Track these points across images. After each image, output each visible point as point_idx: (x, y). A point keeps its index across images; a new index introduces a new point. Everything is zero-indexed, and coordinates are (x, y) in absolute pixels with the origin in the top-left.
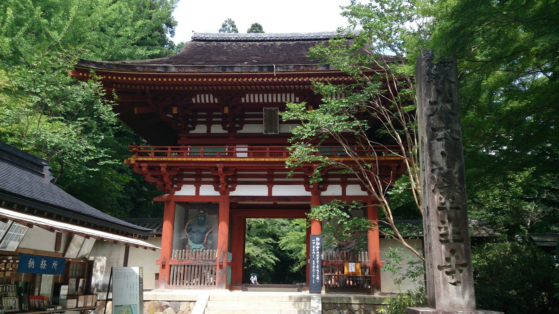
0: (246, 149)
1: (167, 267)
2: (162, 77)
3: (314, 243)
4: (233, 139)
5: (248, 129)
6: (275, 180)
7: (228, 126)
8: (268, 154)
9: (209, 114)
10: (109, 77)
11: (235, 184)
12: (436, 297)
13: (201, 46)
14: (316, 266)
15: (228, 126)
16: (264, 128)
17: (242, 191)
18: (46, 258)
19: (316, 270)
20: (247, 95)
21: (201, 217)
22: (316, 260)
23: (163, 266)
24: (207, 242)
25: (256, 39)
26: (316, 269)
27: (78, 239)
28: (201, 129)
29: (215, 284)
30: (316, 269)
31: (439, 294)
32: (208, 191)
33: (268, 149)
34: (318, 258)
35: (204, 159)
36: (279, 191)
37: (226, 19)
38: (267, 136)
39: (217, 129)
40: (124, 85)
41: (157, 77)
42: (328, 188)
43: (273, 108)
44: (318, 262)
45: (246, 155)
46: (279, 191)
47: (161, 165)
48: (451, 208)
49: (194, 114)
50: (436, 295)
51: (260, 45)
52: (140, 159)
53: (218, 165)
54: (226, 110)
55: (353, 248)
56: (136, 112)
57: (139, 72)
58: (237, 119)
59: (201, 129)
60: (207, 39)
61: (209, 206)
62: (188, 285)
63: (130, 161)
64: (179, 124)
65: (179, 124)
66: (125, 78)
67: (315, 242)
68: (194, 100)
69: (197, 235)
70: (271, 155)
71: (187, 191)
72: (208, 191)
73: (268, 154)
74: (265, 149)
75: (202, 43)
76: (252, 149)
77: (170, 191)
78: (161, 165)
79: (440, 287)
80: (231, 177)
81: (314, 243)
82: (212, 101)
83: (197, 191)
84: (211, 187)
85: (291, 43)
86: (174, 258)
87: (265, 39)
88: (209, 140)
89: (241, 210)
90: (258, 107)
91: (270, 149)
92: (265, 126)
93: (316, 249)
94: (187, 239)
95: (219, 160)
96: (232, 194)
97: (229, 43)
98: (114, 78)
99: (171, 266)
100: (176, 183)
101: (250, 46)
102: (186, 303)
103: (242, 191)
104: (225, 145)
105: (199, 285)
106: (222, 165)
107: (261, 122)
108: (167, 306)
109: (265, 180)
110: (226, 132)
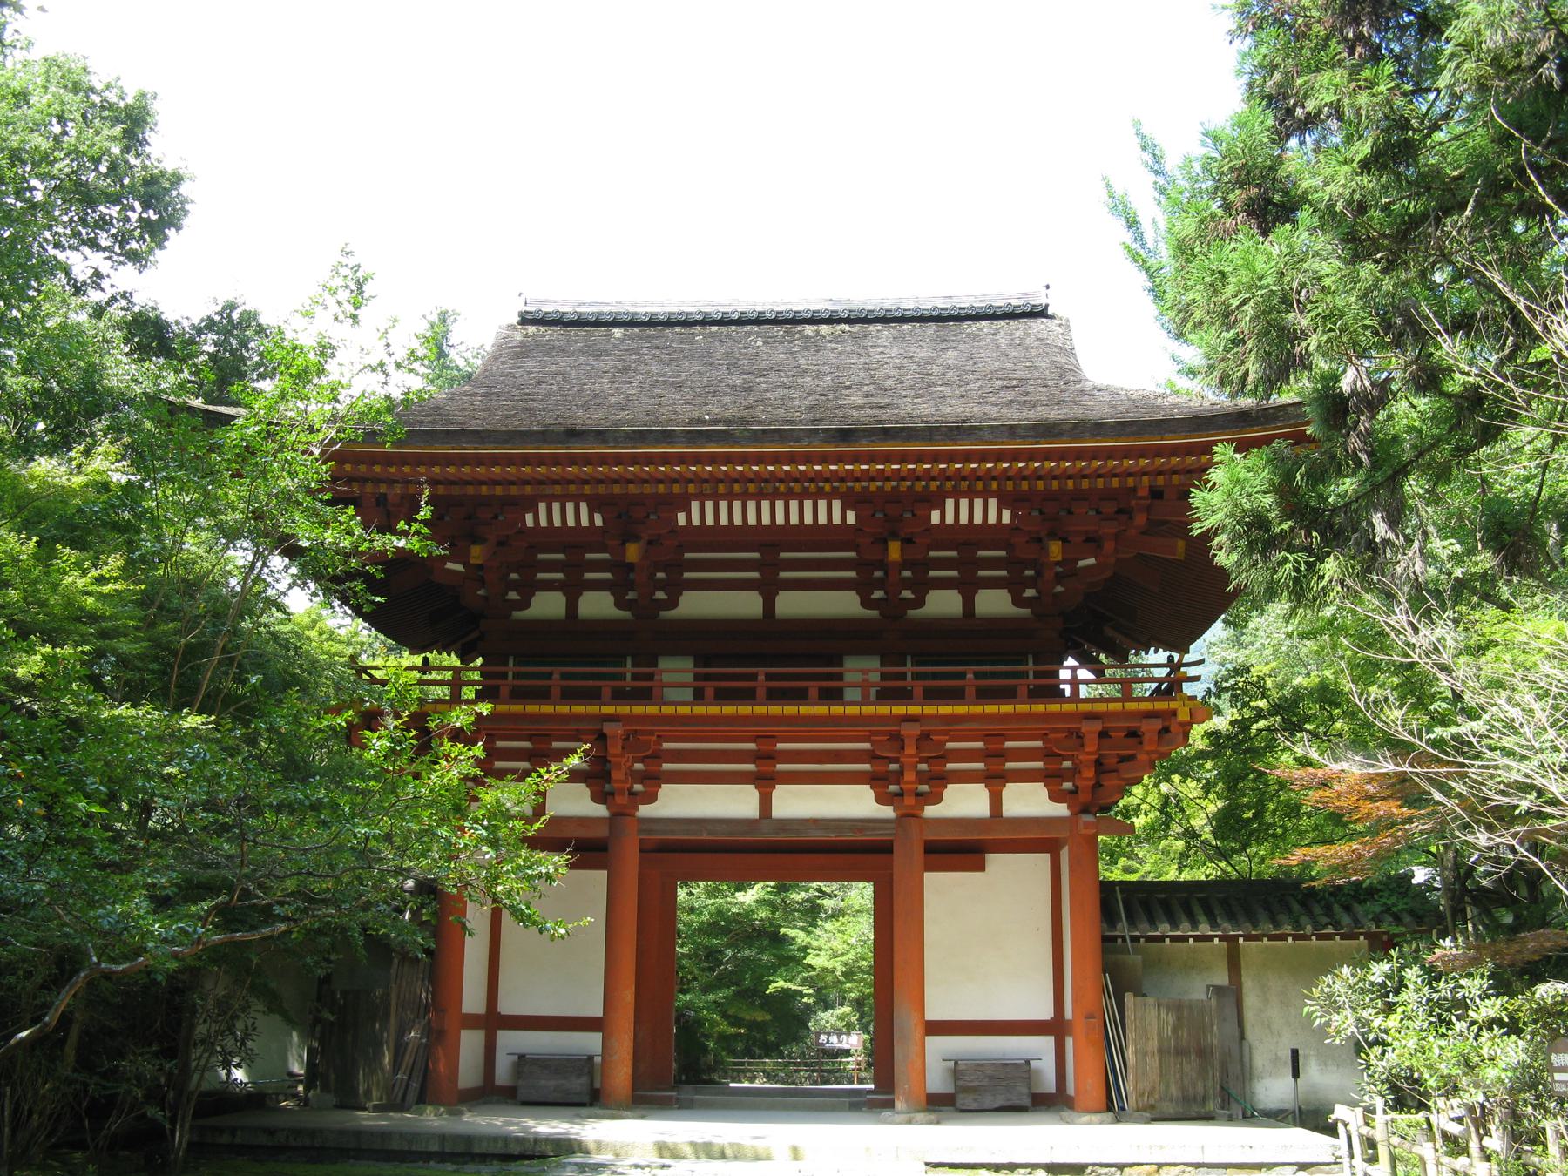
5: (695, 605)
11: (654, 780)
15: (631, 595)
20: (950, 503)
28: (548, 605)
33: (970, 676)
45: (688, 695)
68: (935, 517)
74: (754, 677)
76: (707, 677)
82: (585, 522)
83: (996, 802)
91: (769, 677)
110: (874, 613)
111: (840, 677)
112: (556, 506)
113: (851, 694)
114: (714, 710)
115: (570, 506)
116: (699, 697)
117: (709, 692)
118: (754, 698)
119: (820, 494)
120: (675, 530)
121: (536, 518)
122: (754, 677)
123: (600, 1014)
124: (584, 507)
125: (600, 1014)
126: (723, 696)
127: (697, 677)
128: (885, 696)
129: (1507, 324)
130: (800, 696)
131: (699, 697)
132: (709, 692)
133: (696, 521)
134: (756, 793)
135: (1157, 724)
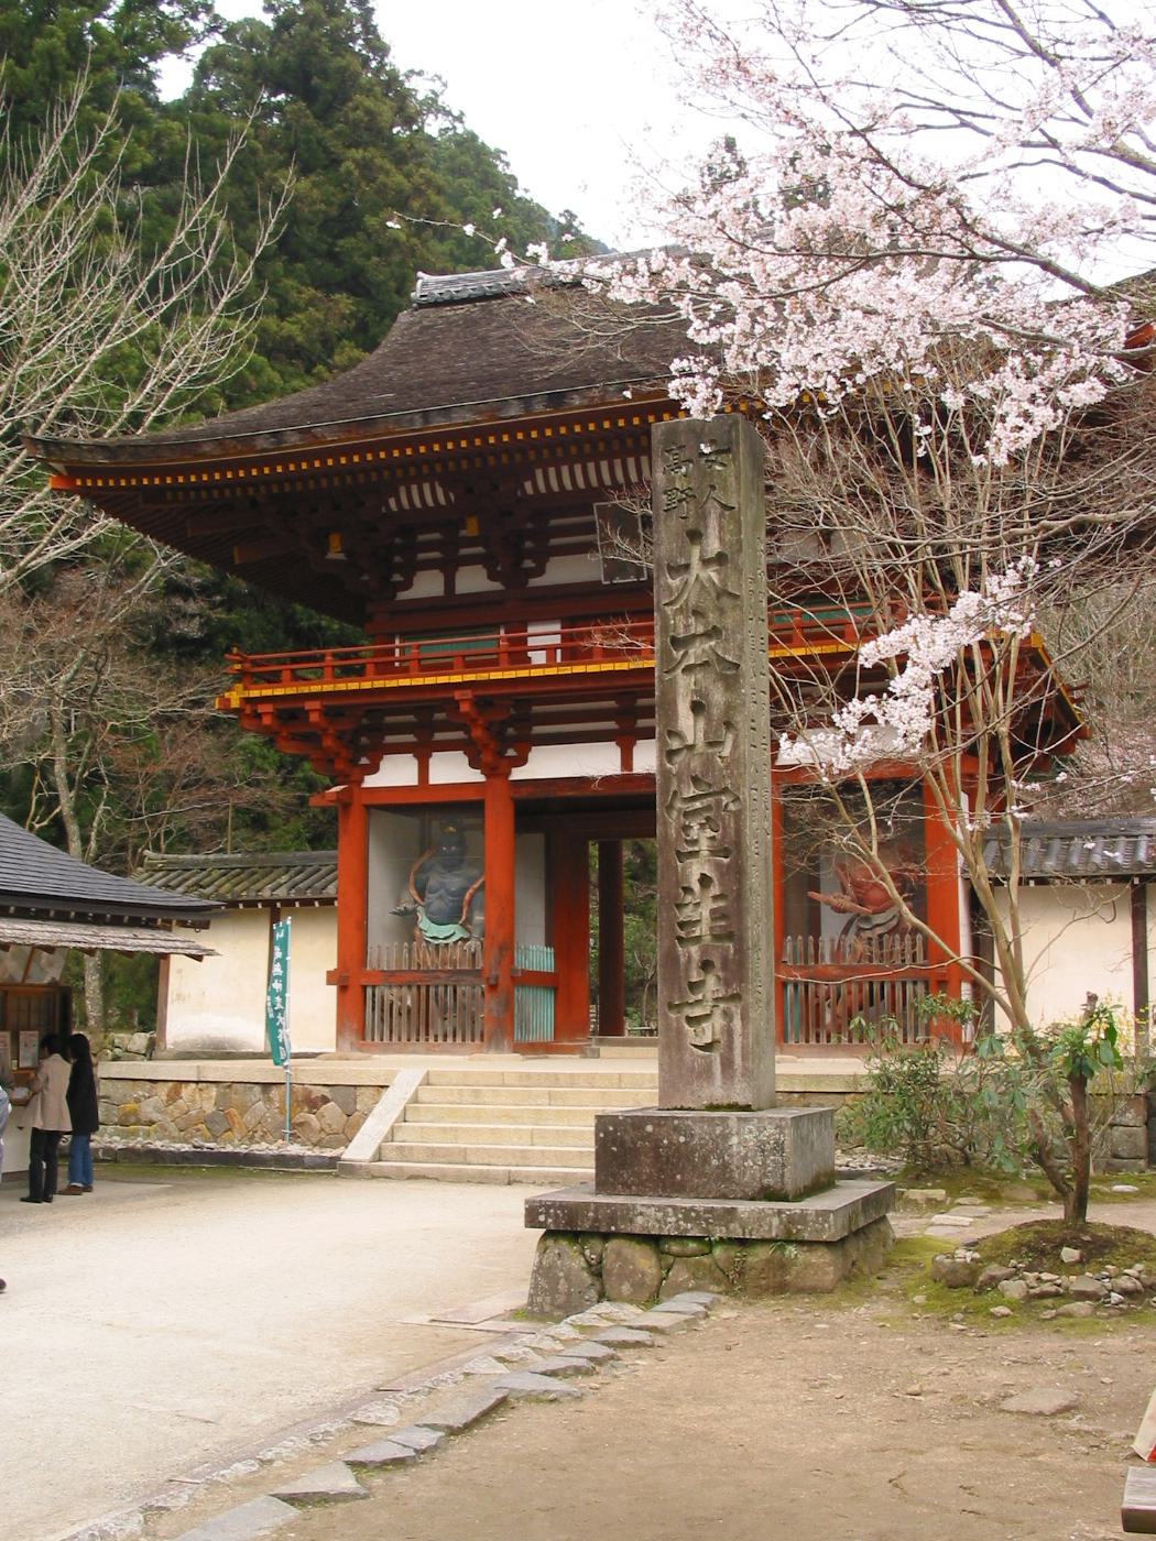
2: (271, 461)
4: (517, 606)
5: (562, 572)
6: (537, 730)
10: (520, 436)
11: (523, 747)
17: (547, 764)
20: (539, 473)
21: (449, 847)
28: (428, 585)
35: (430, 681)
38: (614, 589)
39: (473, 580)
40: (181, 493)
41: (260, 463)
42: (383, 765)
47: (309, 705)
49: (396, 547)
52: (255, 693)
53: (457, 695)
57: (213, 456)
59: (428, 585)
61: (458, 806)
63: (229, 700)
64: (366, 578)
65: (366, 578)
66: (382, 455)
68: (528, 486)
69: (441, 897)
70: (336, 679)
71: (396, 773)
72: (452, 770)
73: (370, 669)
77: (348, 776)
78: (309, 705)
80: (513, 721)
84: (460, 758)
88: (454, 614)
95: (456, 679)
96: (518, 774)
98: (382, 455)
100: (364, 751)
102: (371, 1090)
103: (547, 764)
104: (494, 627)
105: (450, 1040)
106: (469, 694)
108: (325, 1100)
109: (611, 725)
121: (398, 502)
127: (565, 637)
134: (416, 762)
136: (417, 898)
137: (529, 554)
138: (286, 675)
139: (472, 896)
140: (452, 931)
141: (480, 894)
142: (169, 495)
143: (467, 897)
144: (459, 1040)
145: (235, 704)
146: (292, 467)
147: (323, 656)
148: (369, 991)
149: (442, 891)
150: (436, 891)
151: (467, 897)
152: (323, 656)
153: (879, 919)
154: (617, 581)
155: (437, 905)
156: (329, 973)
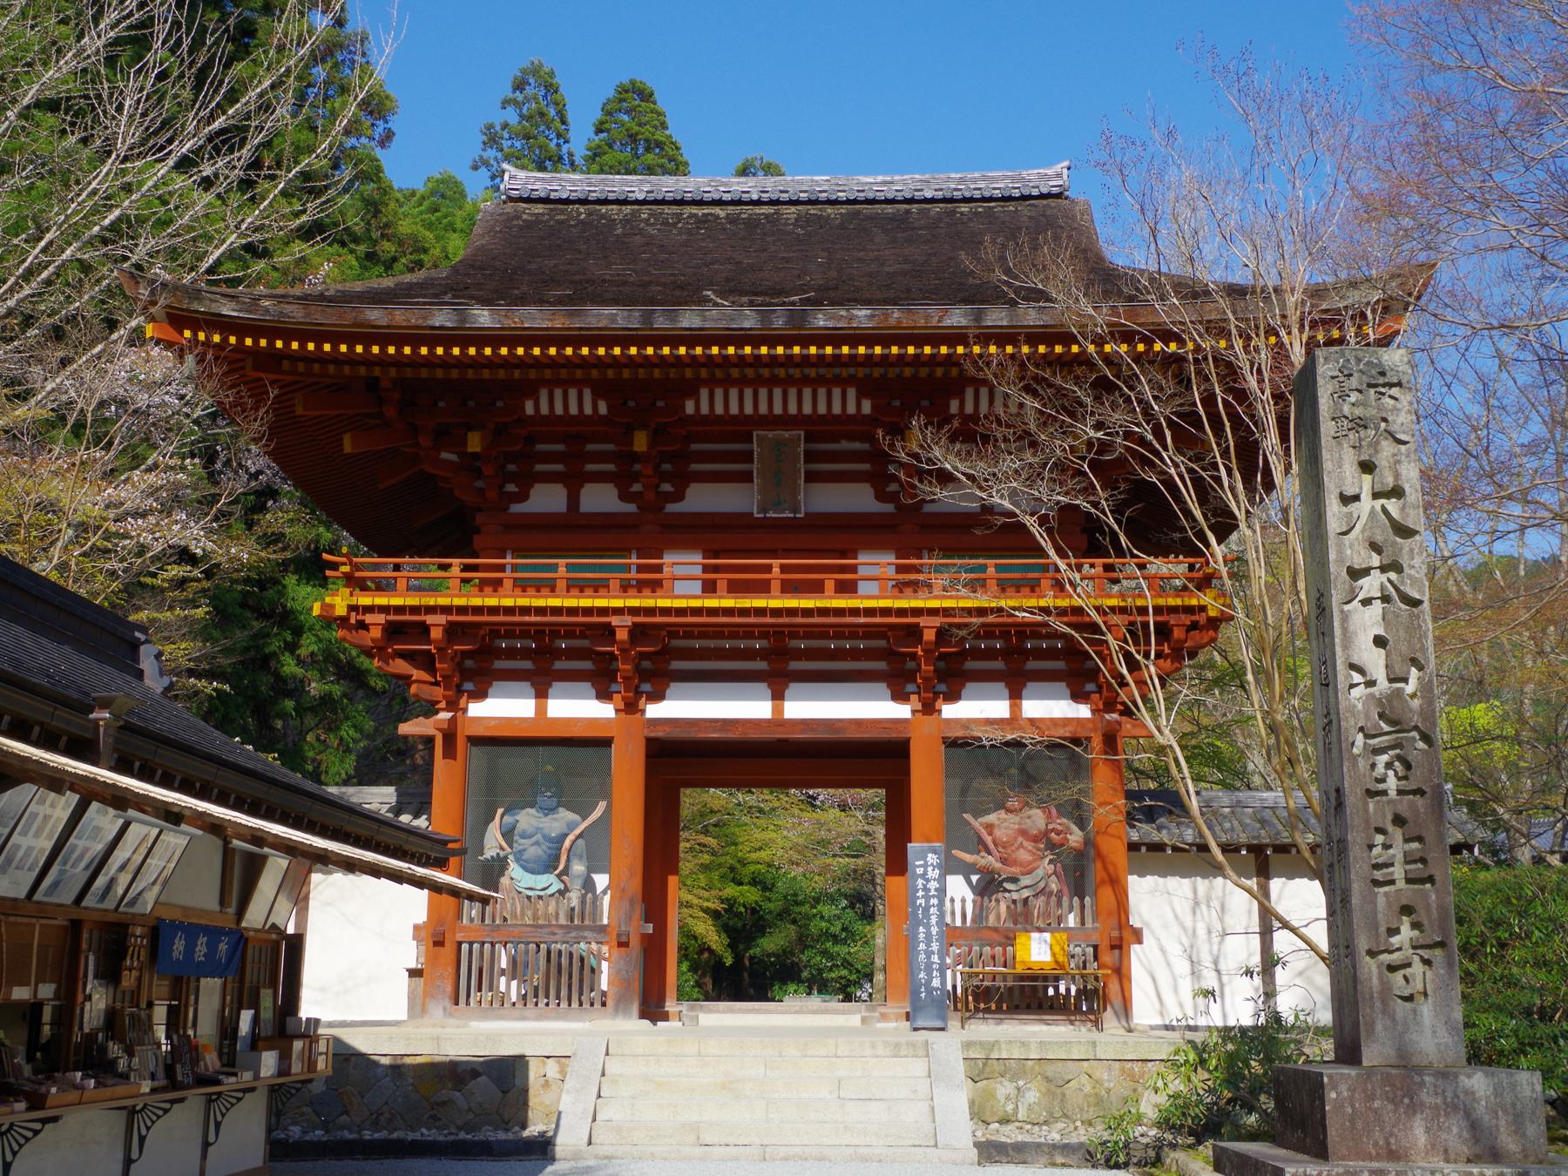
0: (698, 571)
1: (449, 948)
3: (920, 871)
5: (702, 499)
7: (637, 487)
8: (776, 586)
9: (574, 454)
10: (391, 350)
12: (1363, 1034)
13: (537, 221)
14: (928, 945)
15: (637, 487)
16: (757, 497)
17: (682, 707)
18: (206, 930)
19: (928, 957)
20: (704, 393)
22: (928, 926)
23: (439, 943)
24: (567, 867)
25: (716, 196)
26: (929, 954)
27: (277, 864)
28: (547, 499)
29: (604, 1004)
30: (929, 954)
31: (1372, 1025)
32: (577, 707)
34: (934, 920)
36: (810, 707)
37: (526, 65)
39: (600, 499)
40: (316, 366)
43: (787, 434)
44: (934, 930)
45: (697, 587)
46: (810, 707)
48: (1400, 792)
49: (523, 451)
50: (1362, 1027)
51: (732, 219)
52: (365, 600)
54: (641, 442)
55: (1042, 885)
56: (348, 449)
58: (511, 467)
59: (547, 499)
60: (553, 195)
62: (597, 1005)
63: (332, 607)
67: (925, 866)
68: (690, 407)
69: (537, 843)
70: (789, 588)
73: (776, 586)
74: (768, 569)
75: (539, 209)
76: (716, 569)
78: (430, 619)
79: (1372, 1007)
81: (920, 871)
82: (588, 410)
85: (830, 210)
86: (472, 920)
87: (745, 197)
89: (680, 760)
90: (740, 428)
91: (784, 569)
92: (760, 492)
93: (926, 889)
94: (506, 857)
97: (627, 209)
99: (460, 944)
101: (704, 220)
103: (682, 707)
105: (564, 1005)
106: (628, 620)
107: (746, 477)
110: (631, 508)
111: (853, 569)
112: (558, 393)
113: (863, 587)
114: (728, 603)
115: (573, 393)
116: (709, 588)
117: (722, 585)
118: (553, 589)
119: (573, 382)
120: (524, 420)
122: (768, 569)
123: (949, 878)
124: (587, 394)
125: (949, 878)
126: (736, 588)
127: (706, 569)
128: (901, 587)
129: (15, 241)
130: (816, 588)
131: (709, 588)
132: (722, 585)
133: (545, 410)
135: (1186, 619)
136: (504, 844)
137: (511, 478)
138: (830, 585)
139: (574, 842)
140: (549, 882)
141: (580, 841)
142: (286, 364)
143: (567, 843)
144: (575, 1004)
145: (341, 610)
146: (407, 350)
147: (986, 566)
148: (465, 947)
149: (539, 836)
150: (530, 837)
151: (567, 843)
152: (986, 566)
153: (1026, 881)
154: (771, 514)
155: (533, 852)
156: (416, 928)
